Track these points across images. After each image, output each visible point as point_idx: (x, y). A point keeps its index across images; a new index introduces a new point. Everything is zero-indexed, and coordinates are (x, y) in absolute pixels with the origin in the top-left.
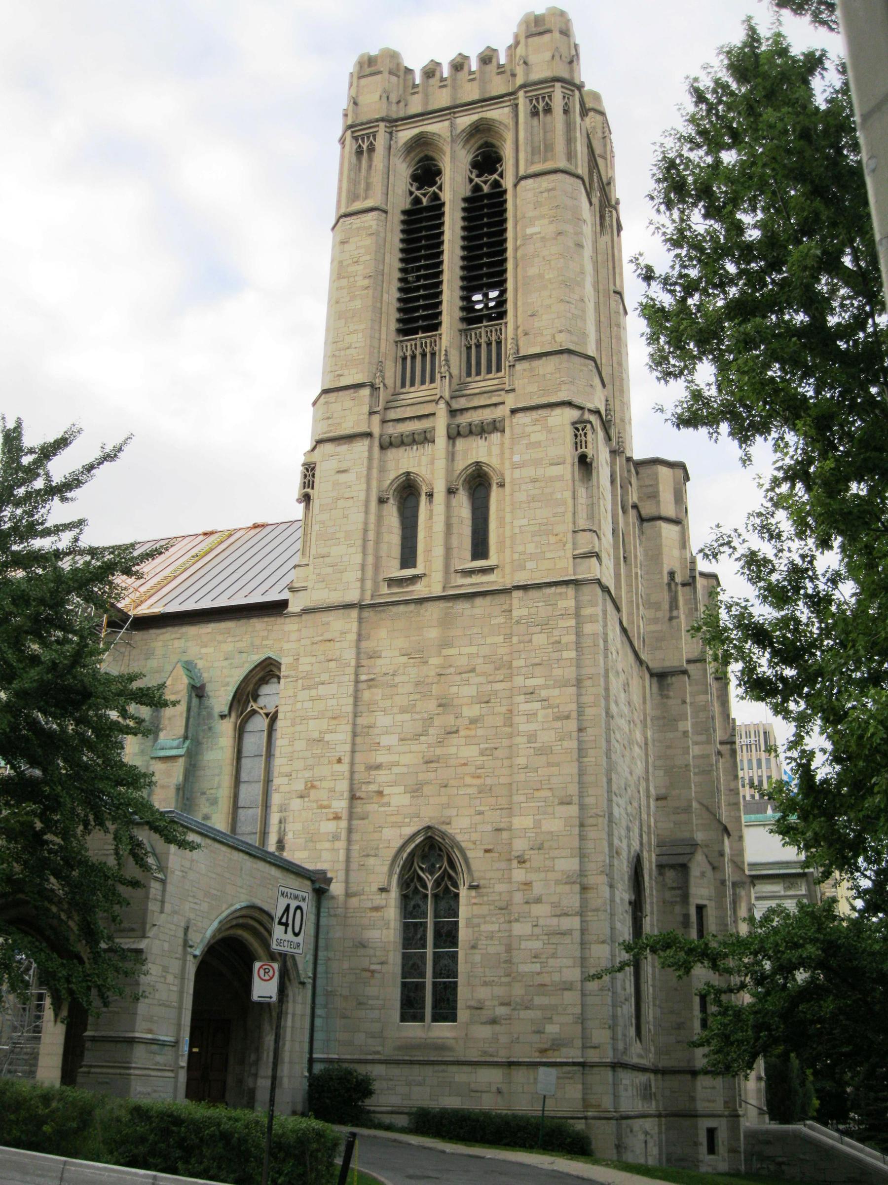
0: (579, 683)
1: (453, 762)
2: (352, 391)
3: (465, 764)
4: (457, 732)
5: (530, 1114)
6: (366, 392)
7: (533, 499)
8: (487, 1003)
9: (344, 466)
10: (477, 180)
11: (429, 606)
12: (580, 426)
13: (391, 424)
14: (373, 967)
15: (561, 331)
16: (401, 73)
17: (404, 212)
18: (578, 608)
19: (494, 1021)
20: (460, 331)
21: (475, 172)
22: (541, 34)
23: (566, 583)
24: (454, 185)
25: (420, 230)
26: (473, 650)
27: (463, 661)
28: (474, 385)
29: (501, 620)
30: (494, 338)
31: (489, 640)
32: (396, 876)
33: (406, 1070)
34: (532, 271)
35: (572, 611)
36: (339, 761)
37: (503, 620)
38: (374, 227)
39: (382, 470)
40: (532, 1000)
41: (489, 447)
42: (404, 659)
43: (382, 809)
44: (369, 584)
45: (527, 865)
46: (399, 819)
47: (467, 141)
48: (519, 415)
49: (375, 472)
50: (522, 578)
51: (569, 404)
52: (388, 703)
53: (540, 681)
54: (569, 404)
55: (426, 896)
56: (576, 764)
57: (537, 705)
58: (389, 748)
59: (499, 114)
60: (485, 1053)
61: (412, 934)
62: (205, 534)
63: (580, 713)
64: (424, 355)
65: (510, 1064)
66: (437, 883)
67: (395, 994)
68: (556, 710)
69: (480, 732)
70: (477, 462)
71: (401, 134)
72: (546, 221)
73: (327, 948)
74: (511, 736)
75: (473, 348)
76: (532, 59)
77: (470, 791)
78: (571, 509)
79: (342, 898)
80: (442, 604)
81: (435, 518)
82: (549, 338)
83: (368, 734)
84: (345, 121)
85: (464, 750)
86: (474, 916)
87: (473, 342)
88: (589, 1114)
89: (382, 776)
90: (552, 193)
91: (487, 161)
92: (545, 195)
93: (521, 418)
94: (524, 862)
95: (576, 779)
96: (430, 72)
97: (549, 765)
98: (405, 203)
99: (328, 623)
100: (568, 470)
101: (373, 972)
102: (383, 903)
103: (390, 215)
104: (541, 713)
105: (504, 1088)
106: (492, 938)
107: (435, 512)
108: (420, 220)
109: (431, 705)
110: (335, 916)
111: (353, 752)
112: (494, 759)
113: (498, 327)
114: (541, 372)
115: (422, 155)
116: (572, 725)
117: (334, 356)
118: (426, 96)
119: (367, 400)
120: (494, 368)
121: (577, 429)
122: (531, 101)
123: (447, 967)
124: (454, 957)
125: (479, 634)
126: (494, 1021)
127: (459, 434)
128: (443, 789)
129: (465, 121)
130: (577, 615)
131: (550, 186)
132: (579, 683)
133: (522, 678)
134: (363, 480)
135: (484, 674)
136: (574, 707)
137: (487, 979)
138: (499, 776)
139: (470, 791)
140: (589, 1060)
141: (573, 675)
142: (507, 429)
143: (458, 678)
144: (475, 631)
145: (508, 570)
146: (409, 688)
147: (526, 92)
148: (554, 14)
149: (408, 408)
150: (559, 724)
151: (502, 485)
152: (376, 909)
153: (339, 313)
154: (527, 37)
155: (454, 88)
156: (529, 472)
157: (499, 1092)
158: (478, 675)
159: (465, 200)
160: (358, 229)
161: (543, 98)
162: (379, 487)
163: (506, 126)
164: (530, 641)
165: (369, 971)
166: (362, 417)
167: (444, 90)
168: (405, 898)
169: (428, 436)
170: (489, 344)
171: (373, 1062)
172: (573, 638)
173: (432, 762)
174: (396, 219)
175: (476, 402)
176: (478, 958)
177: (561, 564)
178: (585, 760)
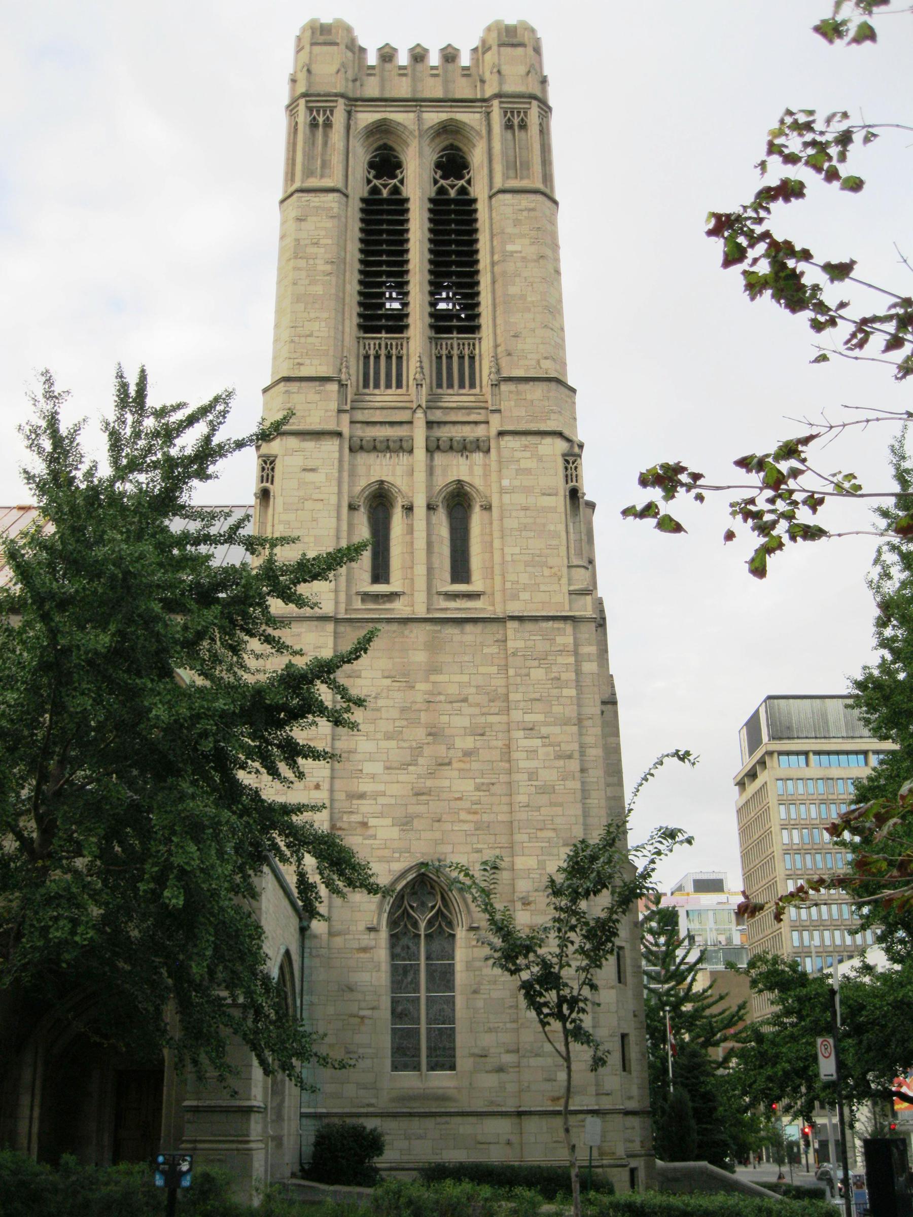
0: (580, 722)
1: (444, 796)
2: (317, 383)
3: (460, 799)
4: (449, 764)
5: (543, 1164)
6: (334, 387)
7: (525, 528)
8: (492, 1050)
9: (310, 464)
10: (442, 182)
11: (413, 626)
12: (571, 459)
13: (359, 425)
14: (362, 1013)
15: (546, 358)
16: (357, 50)
17: (363, 200)
18: (576, 645)
19: (500, 1070)
20: (430, 338)
21: (439, 173)
22: (513, 45)
23: (565, 618)
24: (417, 182)
25: (381, 221)
26: (465, 678)
27: (453, 690)
28: (448, 398)
29: (494, 650)
30: (466, 352)
31: (482, 670)
32: (386, 915)
33: (404, 1123)
34: (513, 290)
35: (571, 648)
36: (317, 787)
37: (496, 651)
38: (335, 210)
39: (353, 474)
40: (542, 1046)
41: (471, 468)
42: (387, 682)
43: (367, 842)
44: (342, 597)
45: (533, 907)
46: (386, 853)
47: (433, 139)
48: (507, 438)
49: (346, 475)
50: (515, 608)
51: (560, 434)
52: (371, 728)
53: (540, 717)
54: (560, 434)
55: (419, 936)
56: (579, 805)
57: (538, 742)
58: (373, 776)
59: (469, 118)
60: (492, 1103)
61: (402, 975)
62: (21, 508)
63: (582, 754)
64: (389, 357)
65: (520, 1114)
66: (430, 923)
67: (386, 1042)
68: (557, 748)
69: (475, 766)
70: (459, 481)
71: (360, 116)
72: (527, 241)
73: (311, 993)
74: (510, 772)
75: (444, 358)
76: (505, 69)
77: (465, 827)
78: (564, 542)
79: (325, 937)
80: (429, 627)
81: (416, 534)
82: (534, 363)
83: (348, 760)
84: (293, 90)
85: (459, 784)
86: (474, 959)
87: (444, 352)
88: (605, 1162)
89: (366, 807)
90: (532, 214)
91: (453, 164)
92: (525, 213)
93: (508, 441)
94: (529, 904)
95: (581, 820)
96: (387, 55)
97: (552, 804)
98: (364, 191)
99: (299, 635)
100: (560, 502)
101: (362, 1018)
102: (373, 943)
103: (350, 200)
104: (541, 751)
105: (515, 1139)
106: (495, 982)
107: (416, 528)
108: (381, 212)
109: (420, 733)
110: (318, 956)
111: (332, 778)
112: (493, 795)
113: (471, 342)
114: (529, 397)
115: (381, 143)
116: (574, 765)
117: (292, 341)
118: (383, 81)
119: (335, 396)
120: (445, 385)
121: (567, 462)
122: (505, 113)
123: (444, 1014)
124: (451, 1001)
125: (470, 665)
126: (500, 1070)
127: (438, 448)
128: (436, 824)
129: (433, 118)
130: (576, 653)
131: (532, 205)
132: (580, 722)
133: (521, 712)
134: (335, 483)
135: (478, 705)
136: (576, 746)
137: (491, 1025)
138: (497, 814)
139: (465, 827)
140: (602, 1107)
141: (574, 715)
142: (493, 451)
143: (449, 706)
144: (466, 658)
145: (498, 597)
146: (395, 714)
147: (307, 102)
148: (526, 29)
149: (378, 412)
150: (561, 763)
151: (488, 508)
152: (365, 950)
153: (294, 298)
154: (500, 45)
155: (414, 79)
156: (520, 499)
157: (509, 1143)
158: (470, 706)
159: (431, 200)
160: (317, 208)
161: (325, 112)
162: (349, 491)
163: (478, 133)
164: (528, 675)
165: (358, 1017)
166: (330, 414)
167: (404, 78)
168: (394, 938)
169: (405, 445)
170: (461, 357)
171: (367, 1115)
172: (573, 676)
173: (423, 794)
174: (355, 205)
175: (453, 417)
176: (480, 1004)
177: (558, 598)
178: (588, 801)
